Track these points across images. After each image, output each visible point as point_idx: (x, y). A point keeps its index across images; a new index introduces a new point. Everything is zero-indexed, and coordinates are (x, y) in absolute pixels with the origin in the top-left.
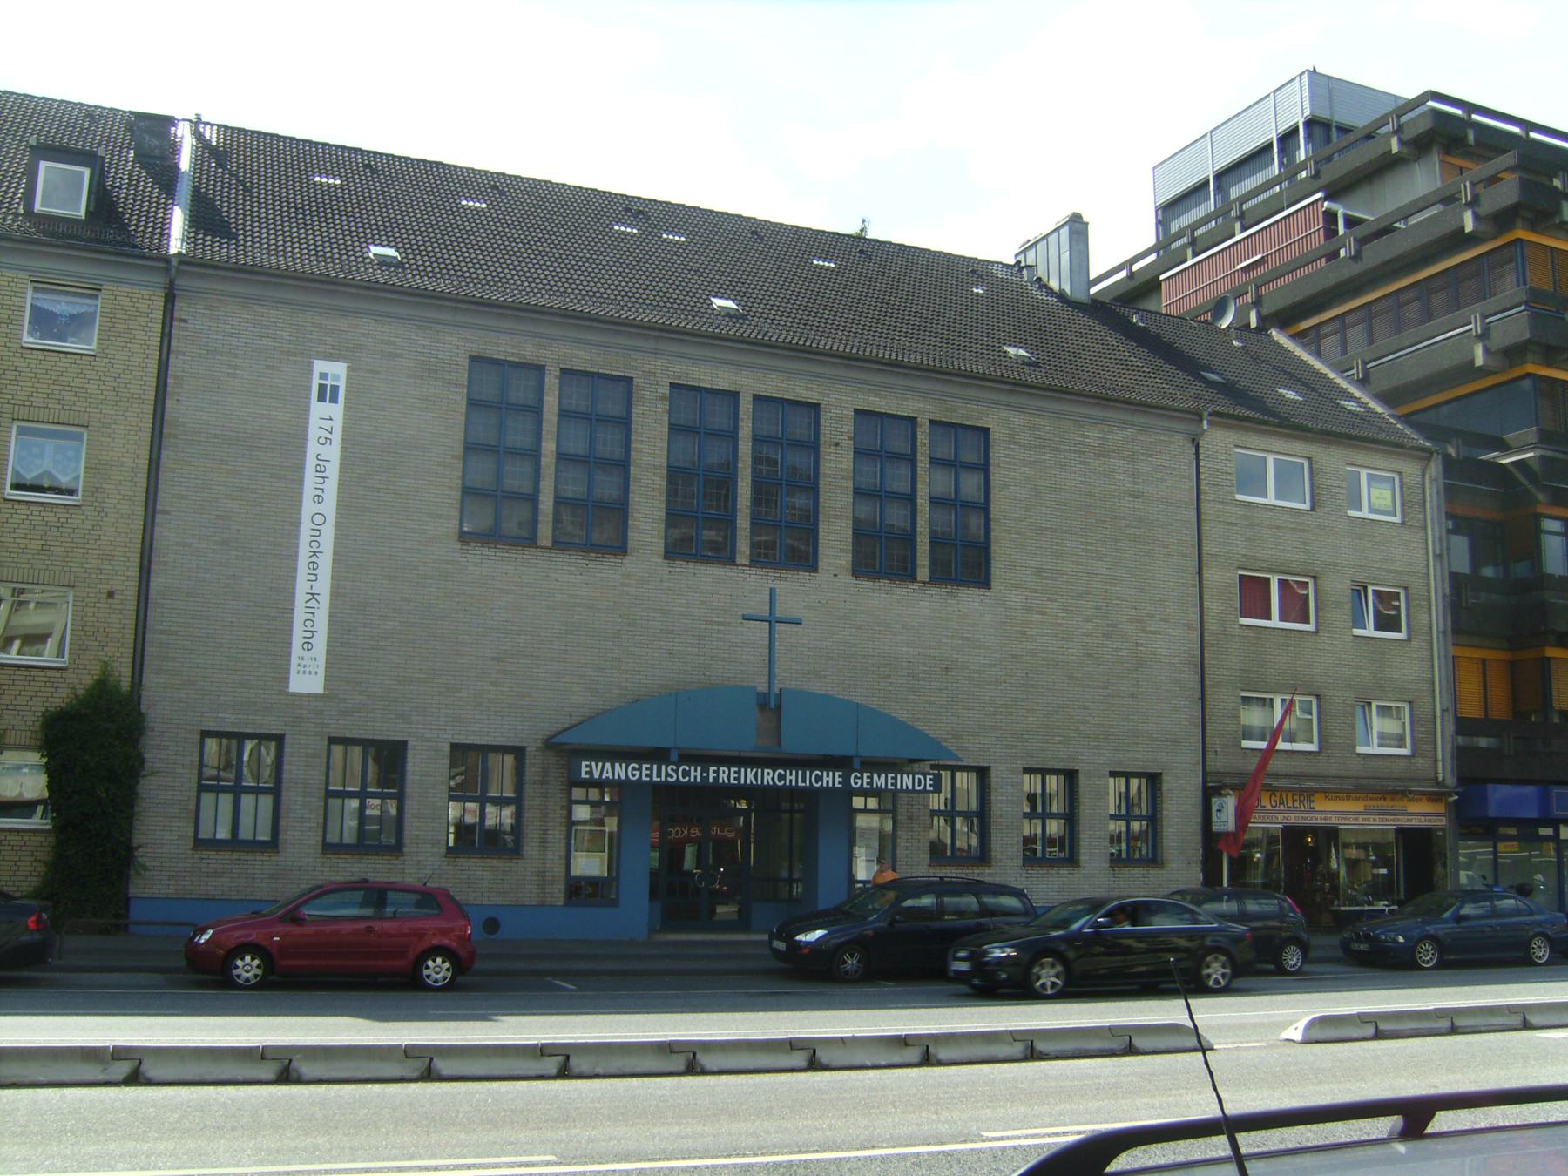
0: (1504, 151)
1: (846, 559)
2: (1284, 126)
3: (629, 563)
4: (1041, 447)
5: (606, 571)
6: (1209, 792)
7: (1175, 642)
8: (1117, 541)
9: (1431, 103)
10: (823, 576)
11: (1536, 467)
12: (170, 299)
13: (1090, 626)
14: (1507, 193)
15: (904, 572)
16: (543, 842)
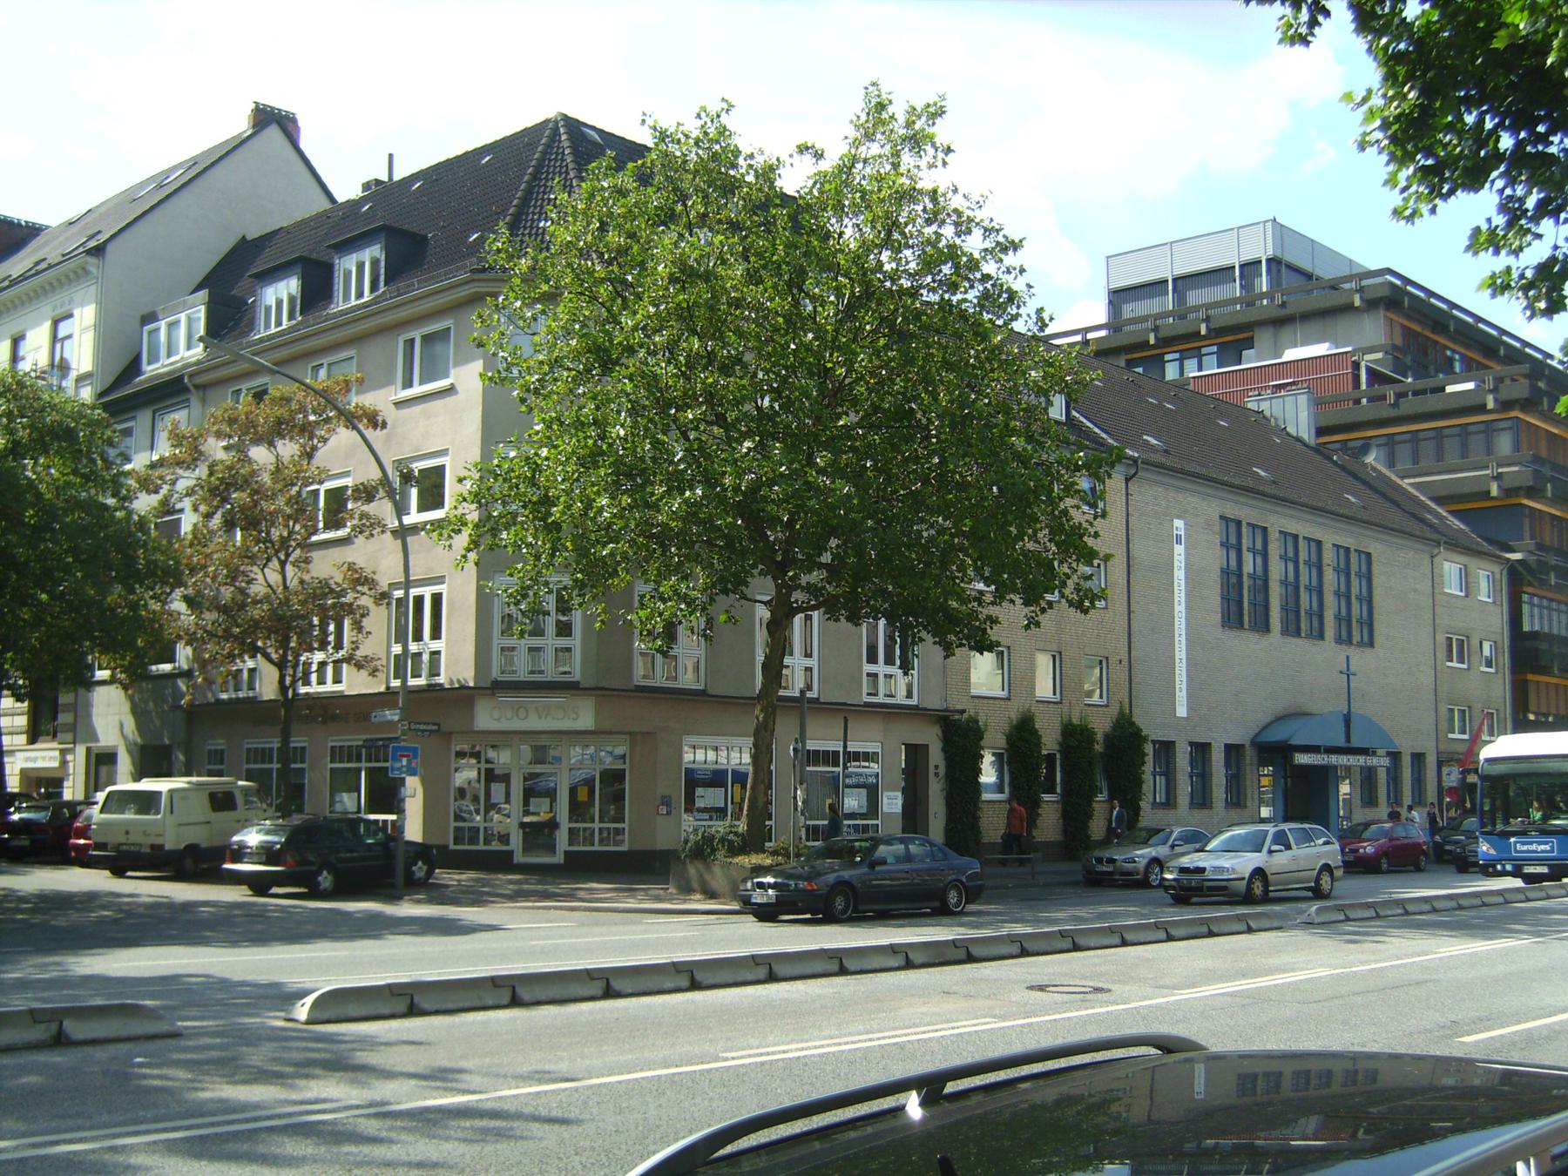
0: (1519, 363)
2: (1248, 256)
6: (1440, 764)
7: (1426, 679)
9: (1389, 277)
11: (1534, 565)
14: (1521, 390)
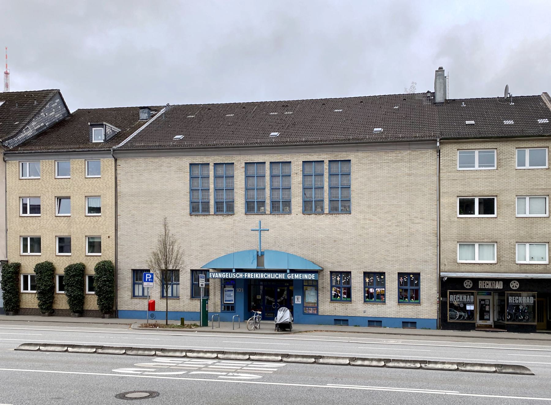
1: (301, 209)
3: (234, 217)
4: (370, 163)
5: (229, 220)
8: (402, 192)
10: (293, 215)
12: (116, 160)
13: (390, 223)
15: (206, 210)
16: (215, 295)
